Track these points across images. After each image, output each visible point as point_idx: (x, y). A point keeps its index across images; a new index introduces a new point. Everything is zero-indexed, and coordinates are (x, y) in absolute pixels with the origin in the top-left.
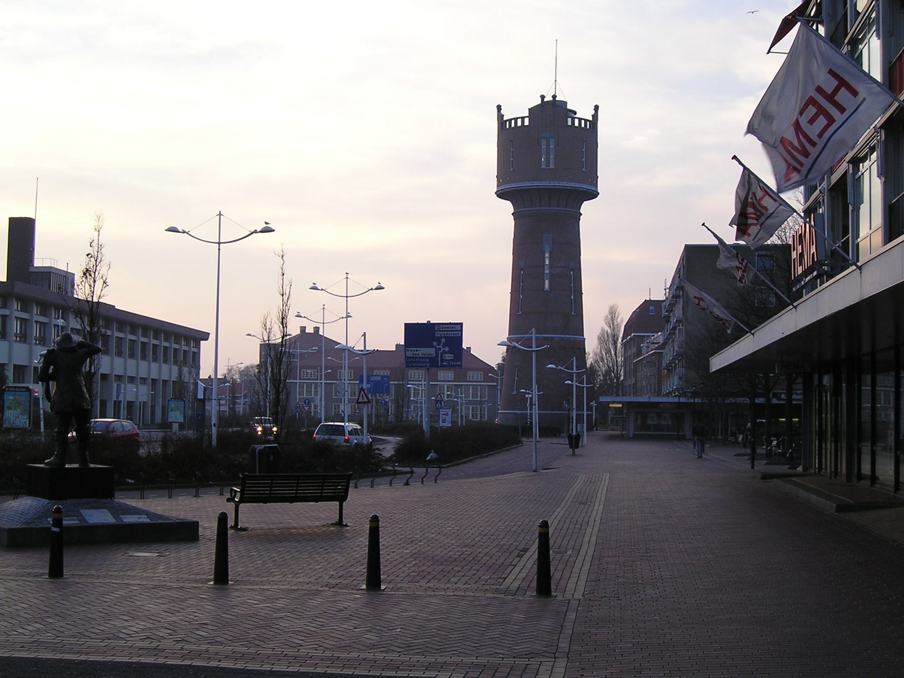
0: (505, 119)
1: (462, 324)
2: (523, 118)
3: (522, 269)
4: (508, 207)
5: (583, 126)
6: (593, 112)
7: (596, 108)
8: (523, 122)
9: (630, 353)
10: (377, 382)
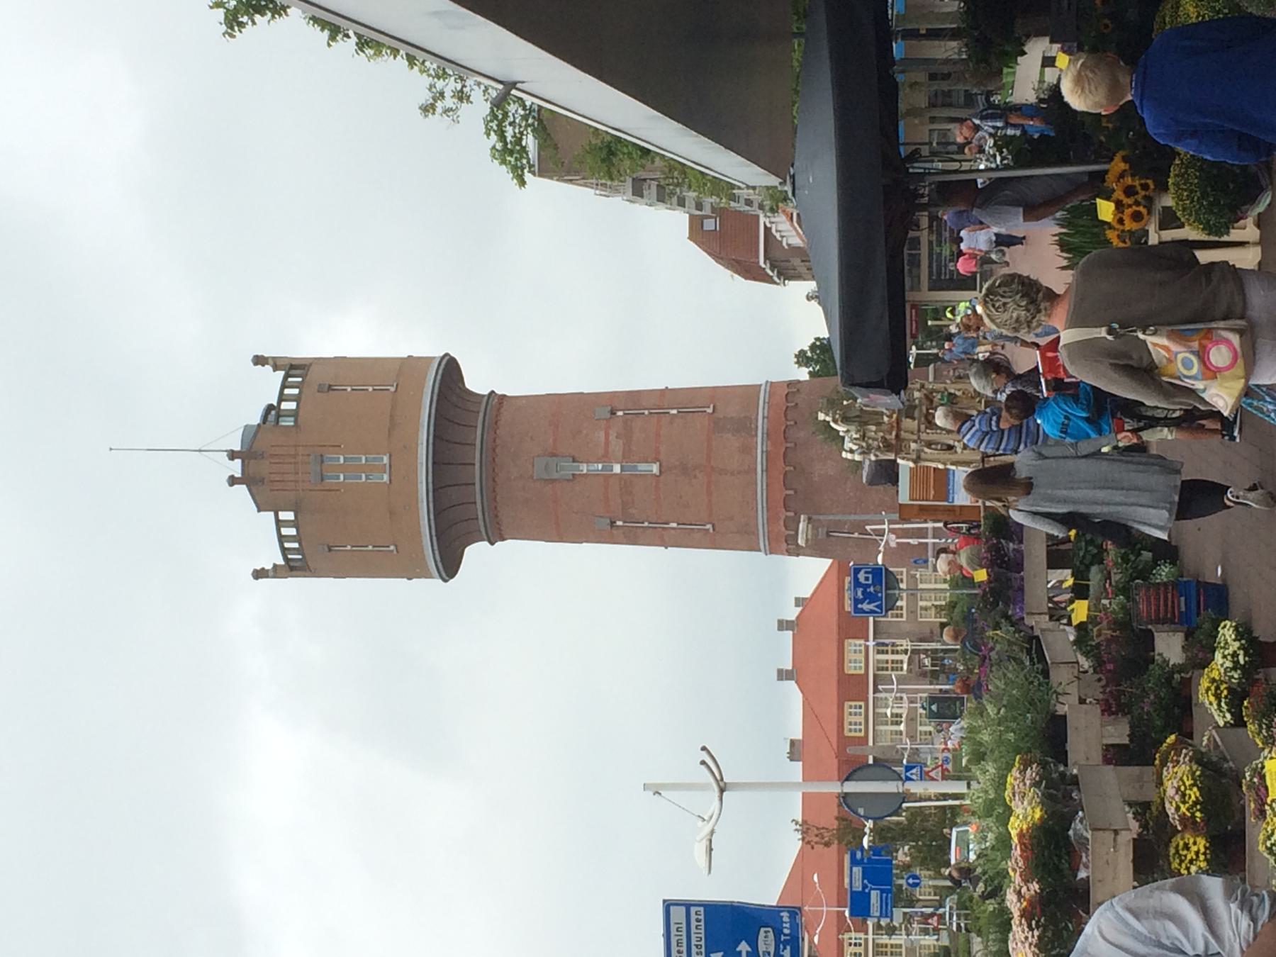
0: (281, 562)
1: (668, 905)
2: (279, 524)
3: (612, 523)
4: (476, 554)
5: (296, 391)
6: (268, 368)
7: (259, 360)
8: (287, 523)
9: (803, 270)
10: (865, 875)
